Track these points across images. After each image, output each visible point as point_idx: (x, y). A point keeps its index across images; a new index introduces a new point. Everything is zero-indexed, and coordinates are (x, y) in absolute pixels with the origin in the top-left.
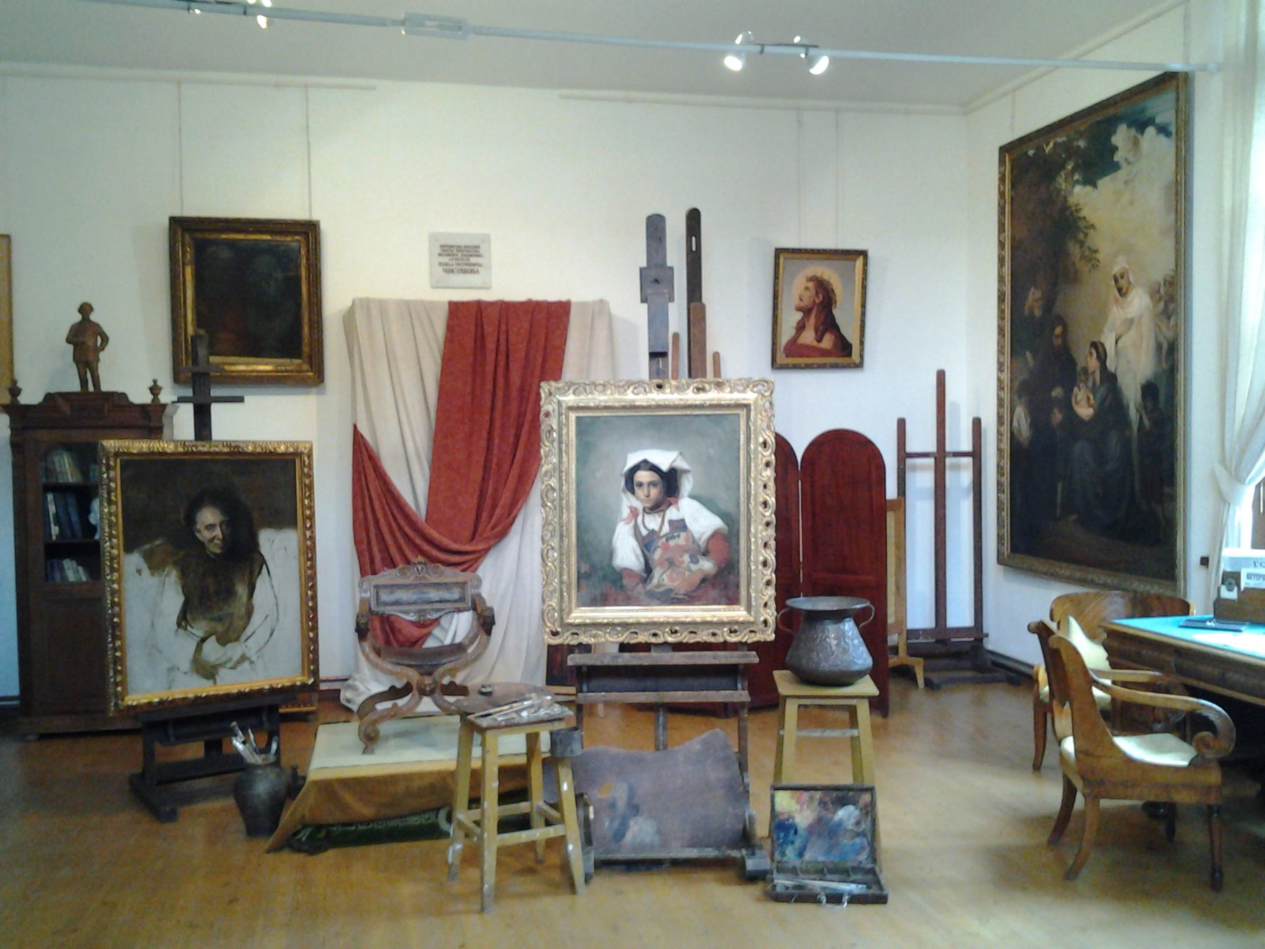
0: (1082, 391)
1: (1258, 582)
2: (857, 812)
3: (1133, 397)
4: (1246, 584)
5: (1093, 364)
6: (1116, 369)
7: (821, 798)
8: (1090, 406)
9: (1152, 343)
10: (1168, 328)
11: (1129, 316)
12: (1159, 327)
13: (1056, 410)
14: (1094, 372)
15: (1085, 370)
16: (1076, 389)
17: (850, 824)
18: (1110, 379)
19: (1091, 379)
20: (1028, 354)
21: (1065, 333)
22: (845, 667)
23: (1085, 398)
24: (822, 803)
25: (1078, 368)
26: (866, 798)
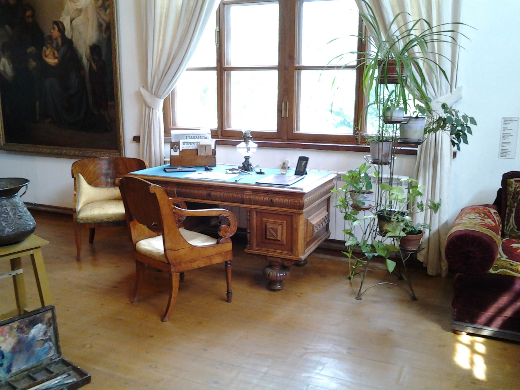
0: (49, 49)
1: (188, 146)
2: (44, 327)
3: (84, 52)
4: (182, 147)
5: (56, 33)
6: (72, 37)
7: (18, 326)
8: (55, 58)
9: (95, 23)
10: (105, 15)
11: (79, 7)
12: (100, 14)
13: (31, 60)
14: (56, 39)
15: (50, 37)
16: (44, 48)
17: (40, 336)
18: (68, 43)
19: (55, 42)
20: (7, 26)
21: (33, 16)
22: (23, 229)
23: (51, 53)
24: (20, 330)
25: (46, 36)
26: (49, 315)
